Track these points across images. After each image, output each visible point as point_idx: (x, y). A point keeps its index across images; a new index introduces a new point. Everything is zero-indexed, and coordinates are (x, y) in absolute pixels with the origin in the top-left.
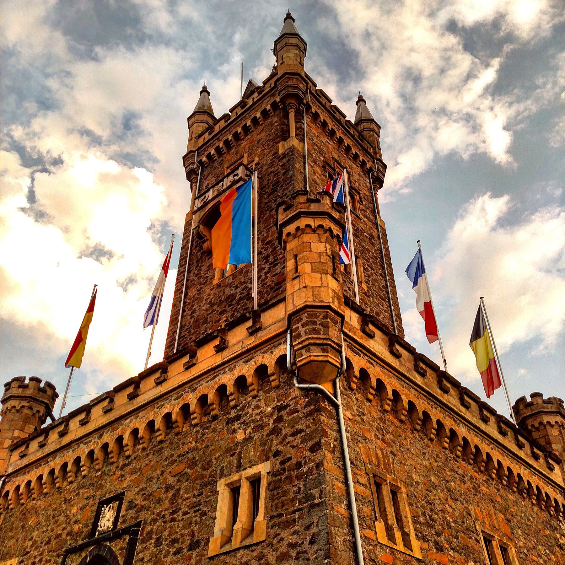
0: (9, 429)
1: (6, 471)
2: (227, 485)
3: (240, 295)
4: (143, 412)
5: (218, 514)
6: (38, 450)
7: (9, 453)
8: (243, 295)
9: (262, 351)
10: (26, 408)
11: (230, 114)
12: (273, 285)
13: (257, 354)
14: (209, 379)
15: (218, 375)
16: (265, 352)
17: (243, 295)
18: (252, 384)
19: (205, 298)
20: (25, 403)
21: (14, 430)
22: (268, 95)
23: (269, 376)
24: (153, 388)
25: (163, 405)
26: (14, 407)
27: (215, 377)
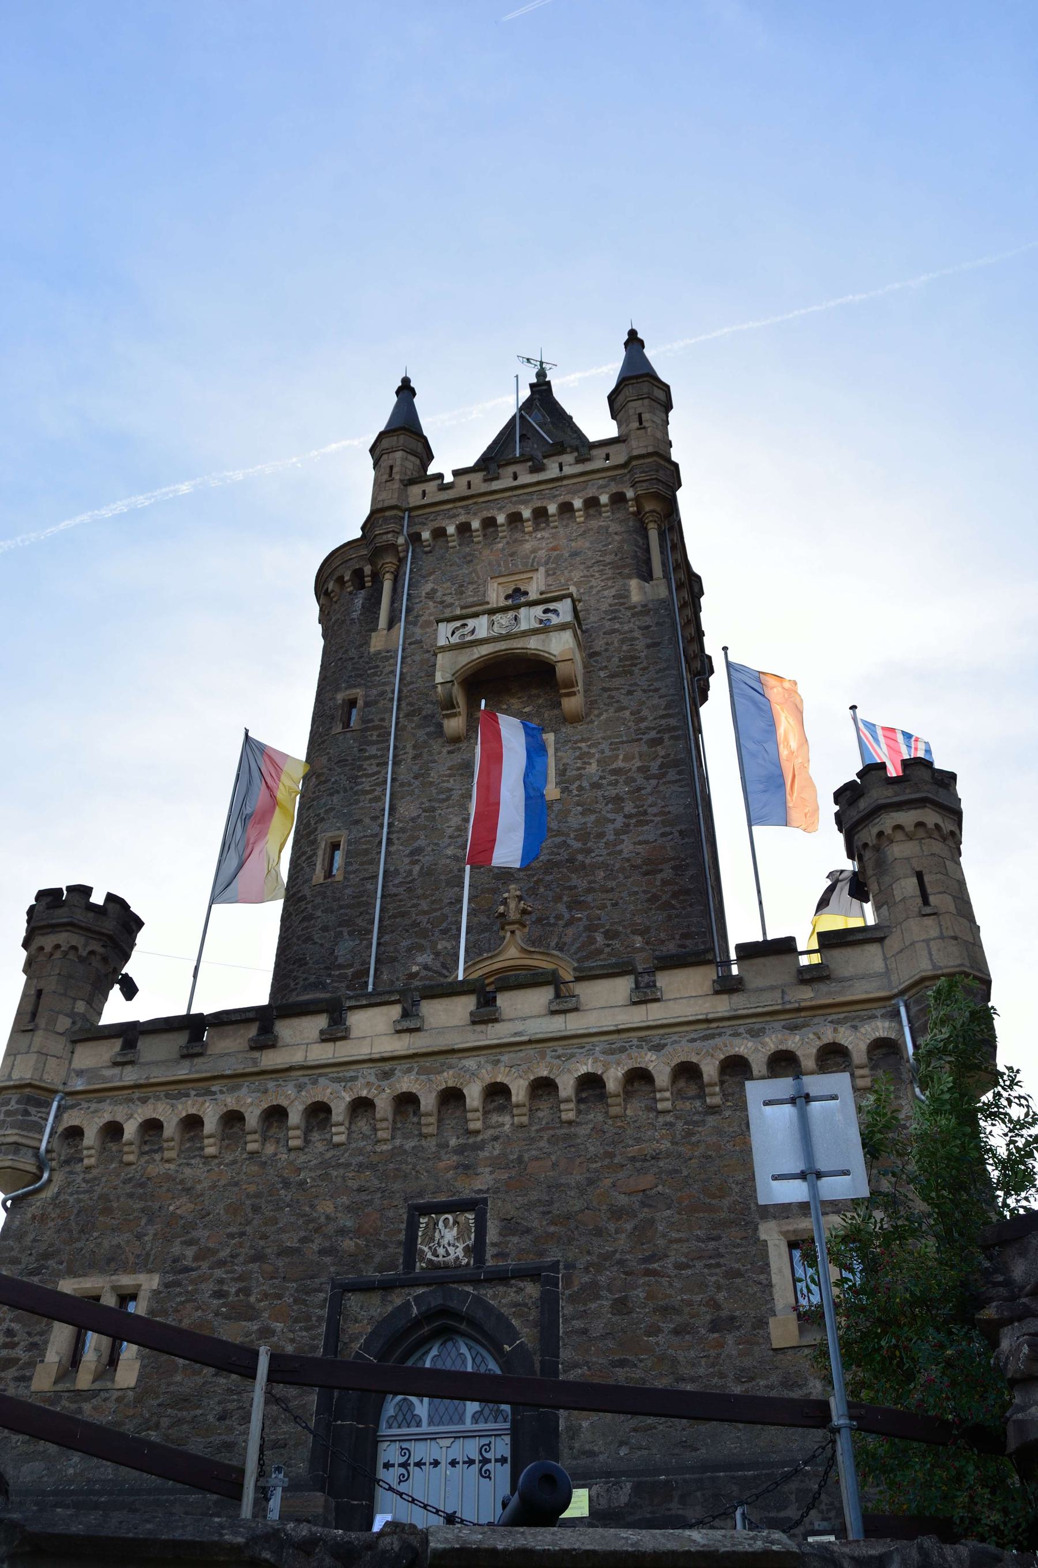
0: (65, 995)
1: (64, 1084)
2: (784, 1234)
3: (550, 854)
4: (512, 1055)
5: (775, 1279)
6: (108, 1067)
7: (69, 1046)
8: (558, 857)
9: (830, 1019)
10: (98, 957)
11: (859, 781)
12: (639, 861)
13: (816, 1020)
14: (693, 1036)
15: (720, 1035)
16: (838, 1022)
17: (558, 857)
18: (172, 1140)
19: (449, 831)
20: (96, 946)
21: (75, 999)
22: (603, 475)
23: (288, 1129)
24: (539, 1017)
25: (573, 1056)
26: (74, 948)
27: (712, 1036)
